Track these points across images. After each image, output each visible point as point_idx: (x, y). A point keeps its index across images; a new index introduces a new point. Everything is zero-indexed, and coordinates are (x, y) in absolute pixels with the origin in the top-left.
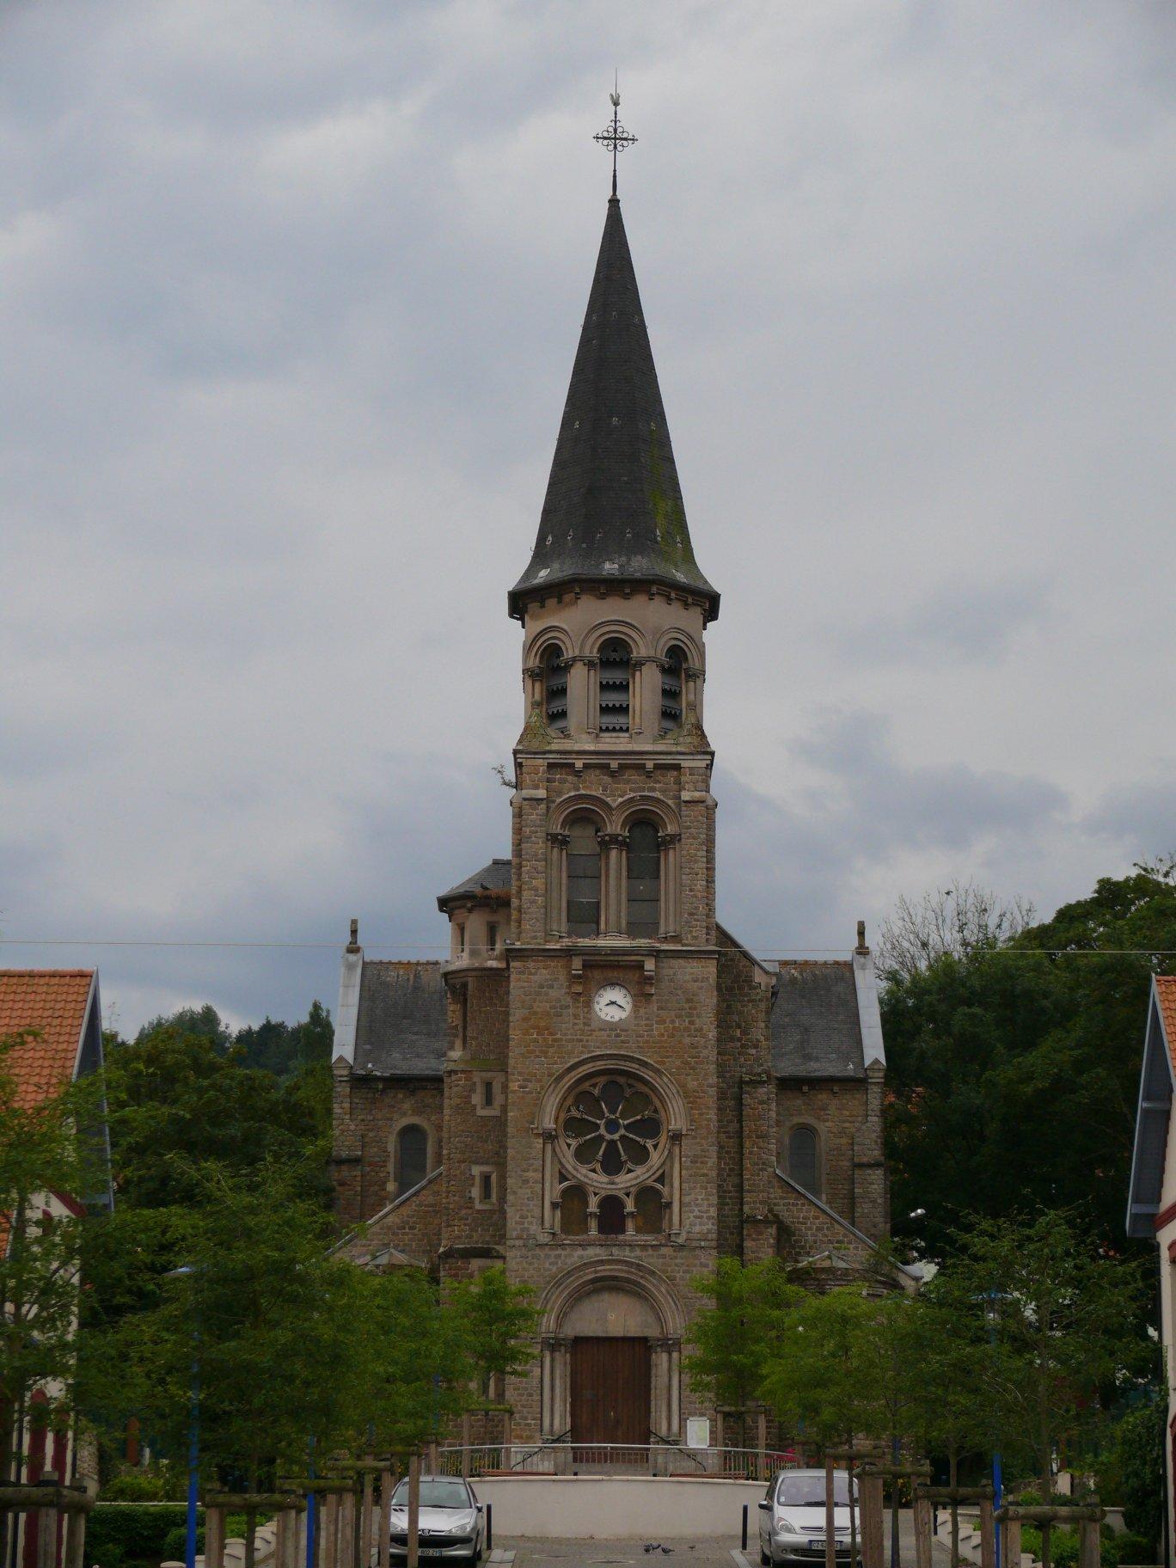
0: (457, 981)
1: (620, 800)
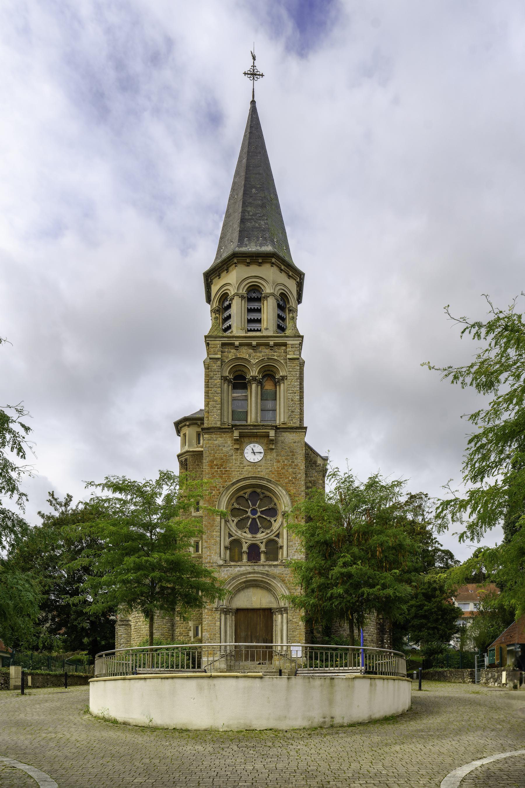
0: (182, 459)
1: (257, 360)
